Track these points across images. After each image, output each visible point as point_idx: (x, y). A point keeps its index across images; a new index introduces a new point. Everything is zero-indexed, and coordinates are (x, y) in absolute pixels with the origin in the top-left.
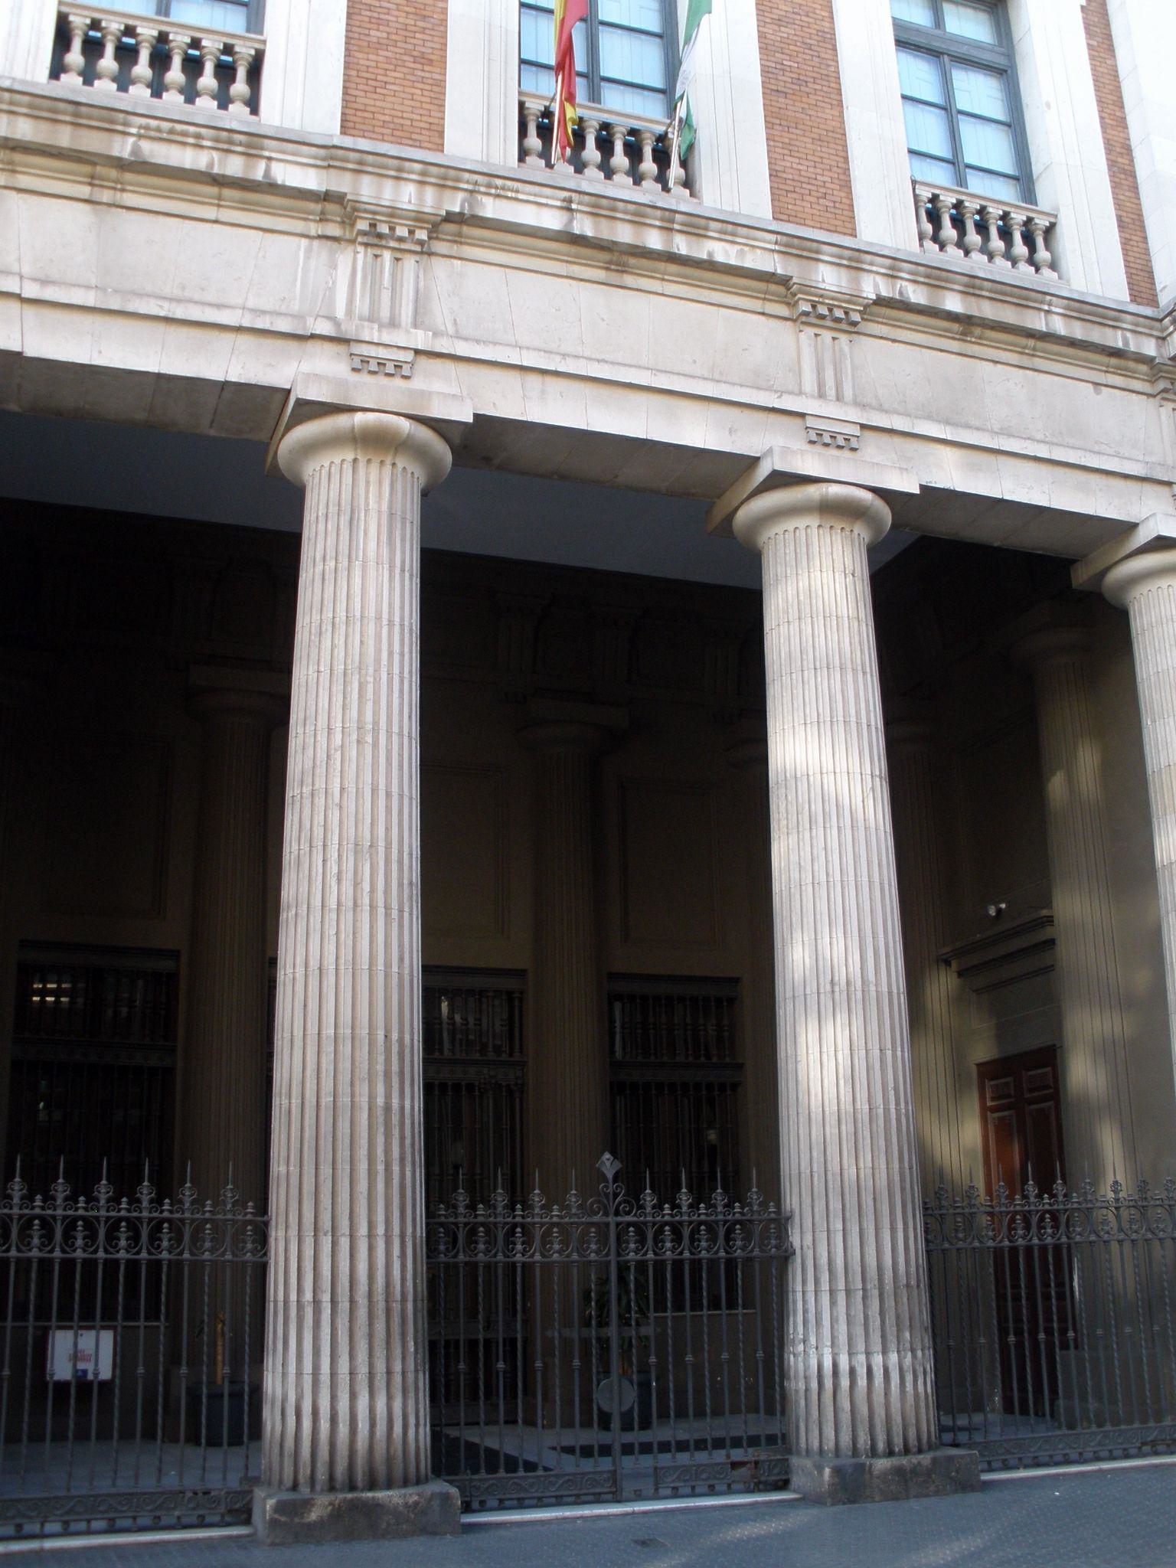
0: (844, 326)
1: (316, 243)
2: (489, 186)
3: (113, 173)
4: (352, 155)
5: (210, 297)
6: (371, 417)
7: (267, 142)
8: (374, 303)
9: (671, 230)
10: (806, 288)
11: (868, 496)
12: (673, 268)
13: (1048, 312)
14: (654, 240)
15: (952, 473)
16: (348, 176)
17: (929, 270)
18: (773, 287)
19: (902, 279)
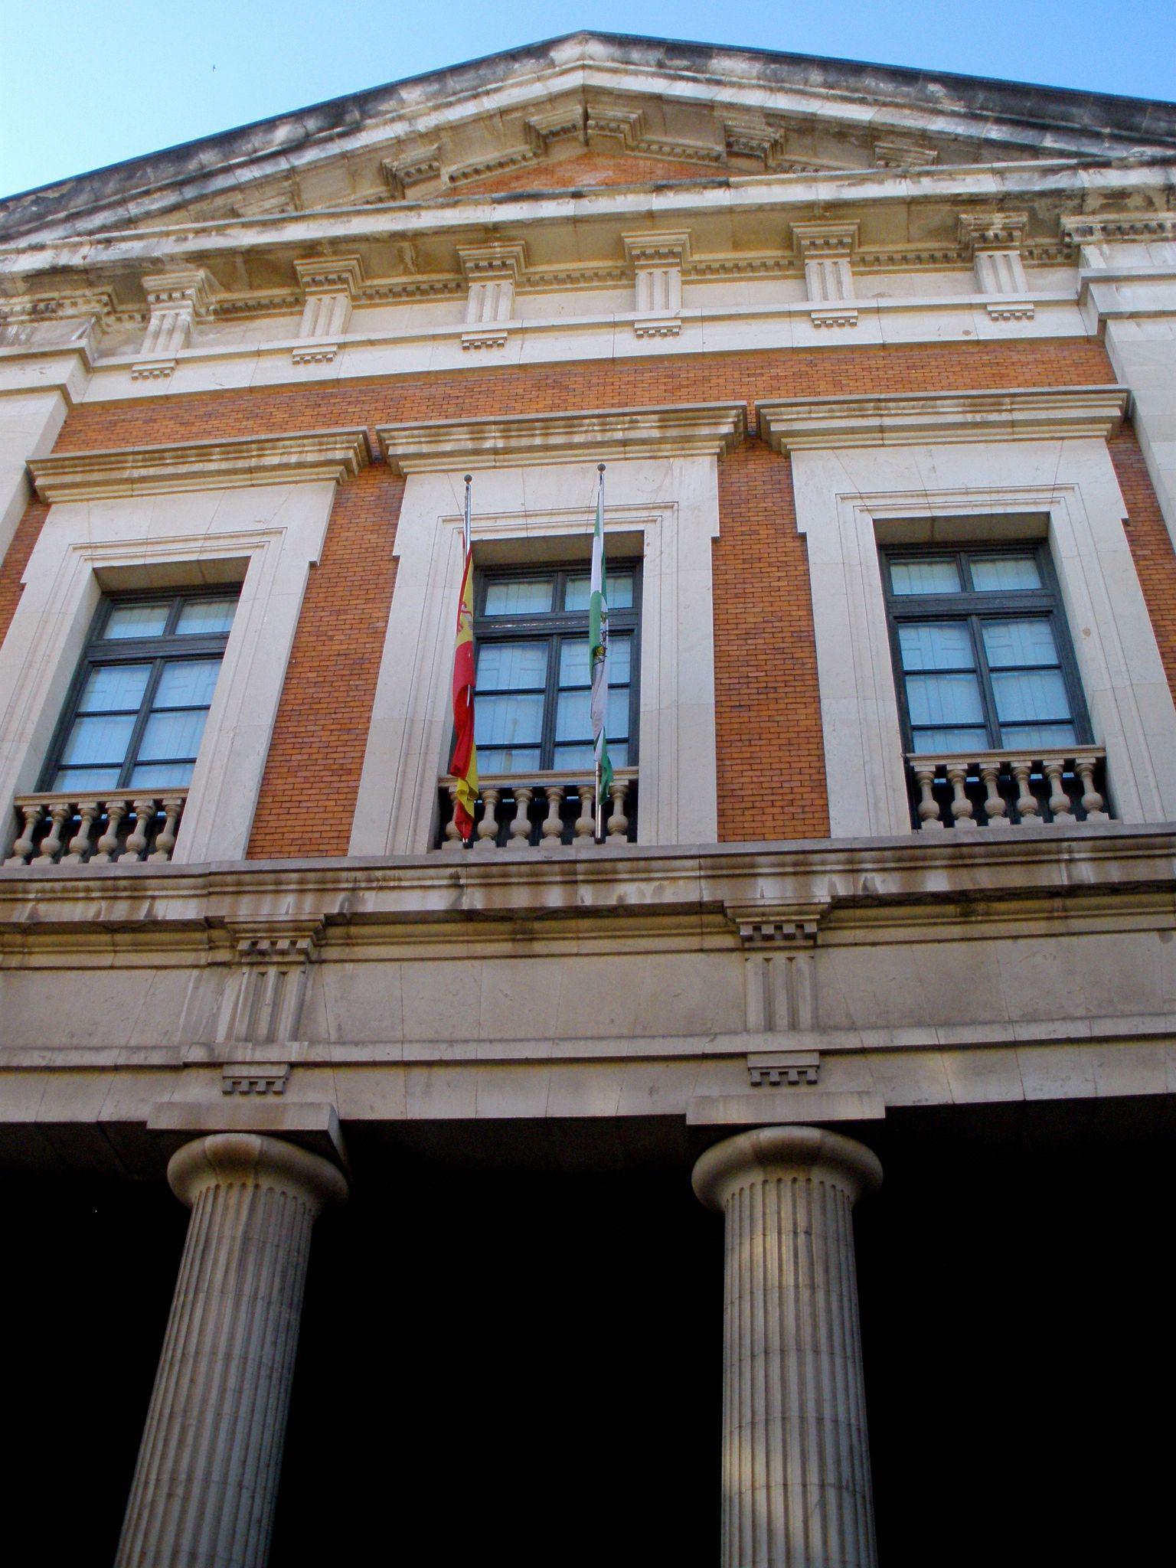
0: (800, 942)
1: (207, 971)
2: (370, 880)
3: (19, 939)
4: (230, 878)
5: (96, 1041)
6: (219, 1139)
7: (148, 881)
8: (253, 1023)
9: (576, 882)
10: (742, 909)
11: (814, 1134)
12: (586, 923)
13: (1071, 861)
14: (554, 898)
15: (945, 1084)
16: (228, 899)
17: (898, 853)
18: (708, 918)
19: (866, 870)
